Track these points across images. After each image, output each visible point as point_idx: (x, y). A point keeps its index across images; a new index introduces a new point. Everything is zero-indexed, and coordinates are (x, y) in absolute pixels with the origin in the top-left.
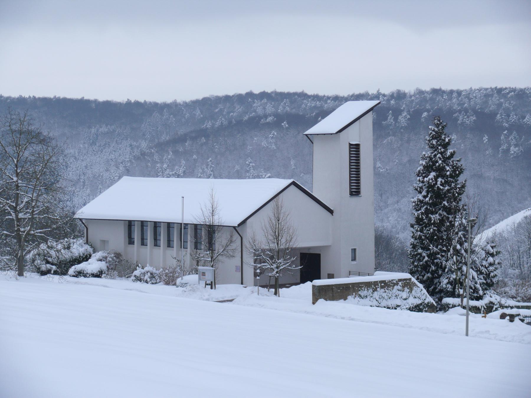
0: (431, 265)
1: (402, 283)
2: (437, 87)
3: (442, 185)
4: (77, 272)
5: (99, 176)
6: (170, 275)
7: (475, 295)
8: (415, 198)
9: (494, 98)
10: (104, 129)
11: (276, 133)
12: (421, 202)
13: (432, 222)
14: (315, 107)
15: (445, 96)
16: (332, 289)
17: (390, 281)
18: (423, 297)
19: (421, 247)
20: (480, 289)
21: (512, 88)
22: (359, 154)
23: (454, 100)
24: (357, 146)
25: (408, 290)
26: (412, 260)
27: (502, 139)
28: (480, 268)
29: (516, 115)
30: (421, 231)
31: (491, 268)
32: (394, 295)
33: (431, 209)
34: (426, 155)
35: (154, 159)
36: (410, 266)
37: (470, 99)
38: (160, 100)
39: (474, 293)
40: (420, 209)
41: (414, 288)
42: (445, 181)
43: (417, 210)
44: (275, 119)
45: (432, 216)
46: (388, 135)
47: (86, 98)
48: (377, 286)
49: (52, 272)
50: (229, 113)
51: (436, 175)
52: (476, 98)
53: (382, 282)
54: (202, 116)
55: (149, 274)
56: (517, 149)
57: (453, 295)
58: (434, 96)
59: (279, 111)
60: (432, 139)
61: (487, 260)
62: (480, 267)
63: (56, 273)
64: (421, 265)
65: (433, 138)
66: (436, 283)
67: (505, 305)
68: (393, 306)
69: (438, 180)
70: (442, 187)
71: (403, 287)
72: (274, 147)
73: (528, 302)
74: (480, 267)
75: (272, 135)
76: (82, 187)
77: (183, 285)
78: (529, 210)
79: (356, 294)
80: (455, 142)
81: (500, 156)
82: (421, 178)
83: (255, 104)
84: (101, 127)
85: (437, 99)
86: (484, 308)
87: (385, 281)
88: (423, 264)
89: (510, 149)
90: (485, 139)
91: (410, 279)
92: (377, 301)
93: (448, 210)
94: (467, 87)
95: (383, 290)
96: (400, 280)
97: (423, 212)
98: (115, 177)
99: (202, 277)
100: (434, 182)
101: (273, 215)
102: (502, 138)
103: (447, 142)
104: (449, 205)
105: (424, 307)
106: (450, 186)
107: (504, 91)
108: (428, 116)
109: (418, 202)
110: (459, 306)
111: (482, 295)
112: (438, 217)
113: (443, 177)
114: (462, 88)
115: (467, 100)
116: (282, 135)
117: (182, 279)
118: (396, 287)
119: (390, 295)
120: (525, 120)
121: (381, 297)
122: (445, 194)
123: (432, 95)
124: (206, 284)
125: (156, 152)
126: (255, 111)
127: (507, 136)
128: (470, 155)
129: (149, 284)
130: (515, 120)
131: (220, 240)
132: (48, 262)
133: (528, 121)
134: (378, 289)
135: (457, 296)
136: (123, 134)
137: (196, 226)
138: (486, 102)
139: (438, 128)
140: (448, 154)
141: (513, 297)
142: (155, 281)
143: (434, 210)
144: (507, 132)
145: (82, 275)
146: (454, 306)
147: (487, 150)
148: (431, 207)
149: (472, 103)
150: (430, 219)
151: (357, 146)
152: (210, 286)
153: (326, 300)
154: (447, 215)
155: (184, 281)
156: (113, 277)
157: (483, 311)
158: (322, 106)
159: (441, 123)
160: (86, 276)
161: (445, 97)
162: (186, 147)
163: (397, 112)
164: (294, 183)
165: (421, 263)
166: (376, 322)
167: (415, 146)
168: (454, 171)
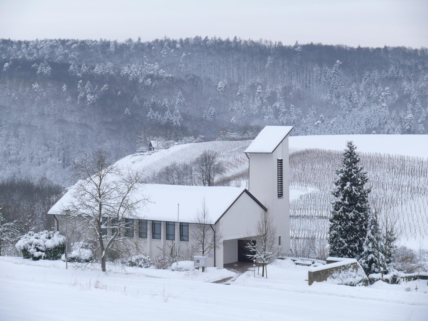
2: (7, 38)
4: (71, 258)
6: (162, 261)
15: (15, 46)
16: (320, 273)
21: (74, 40)
27: (78, 88)
29: (87, 66)
30: (340, 224)
32: (349, 275)
37: (38, 50)
40: (339, 209)
43: (337, 211)
45: (348, 214)
49: (43, 258)
53: (344, 266)
56: (93, 96)
58: (5, 47)
63: (44, 258)
64: (341, 250)
69: (352, 187)
71: (353, 269)
78: (134, 156)
80: (38, 90)
81: (78, 103)
85: (8, 49)
86: (391, 280)
87: (344, 265)
90: (64, 87)
91: (356, 263)
94: (34, 39)
96: (352, 264)
97: (342, 210)
99: (196, 263)
102: (79, 86)
109: (336, 203)
110: (380, 279)
114: (29, 39)
115: (35, 50)
117: (177, 265)
119: (347, 275)
120: (95, 70)
123: (3, 45)
127: (83, 85)
128: (52, 102)
129: (143, 268)
132: (38, 250)
134: (342, 271)
138: (52, 53)
144: (82, 82)
146: (377, 280)
147: (67, 97)
149: (40, 53)
150: (347, 216)
155: (179, 266)
157: (391, 282)
160: (80, 261)
161: (15, 47)
164: (246, 191)
165: (342, 248)
166: (374, 299)
167: (2, 93)
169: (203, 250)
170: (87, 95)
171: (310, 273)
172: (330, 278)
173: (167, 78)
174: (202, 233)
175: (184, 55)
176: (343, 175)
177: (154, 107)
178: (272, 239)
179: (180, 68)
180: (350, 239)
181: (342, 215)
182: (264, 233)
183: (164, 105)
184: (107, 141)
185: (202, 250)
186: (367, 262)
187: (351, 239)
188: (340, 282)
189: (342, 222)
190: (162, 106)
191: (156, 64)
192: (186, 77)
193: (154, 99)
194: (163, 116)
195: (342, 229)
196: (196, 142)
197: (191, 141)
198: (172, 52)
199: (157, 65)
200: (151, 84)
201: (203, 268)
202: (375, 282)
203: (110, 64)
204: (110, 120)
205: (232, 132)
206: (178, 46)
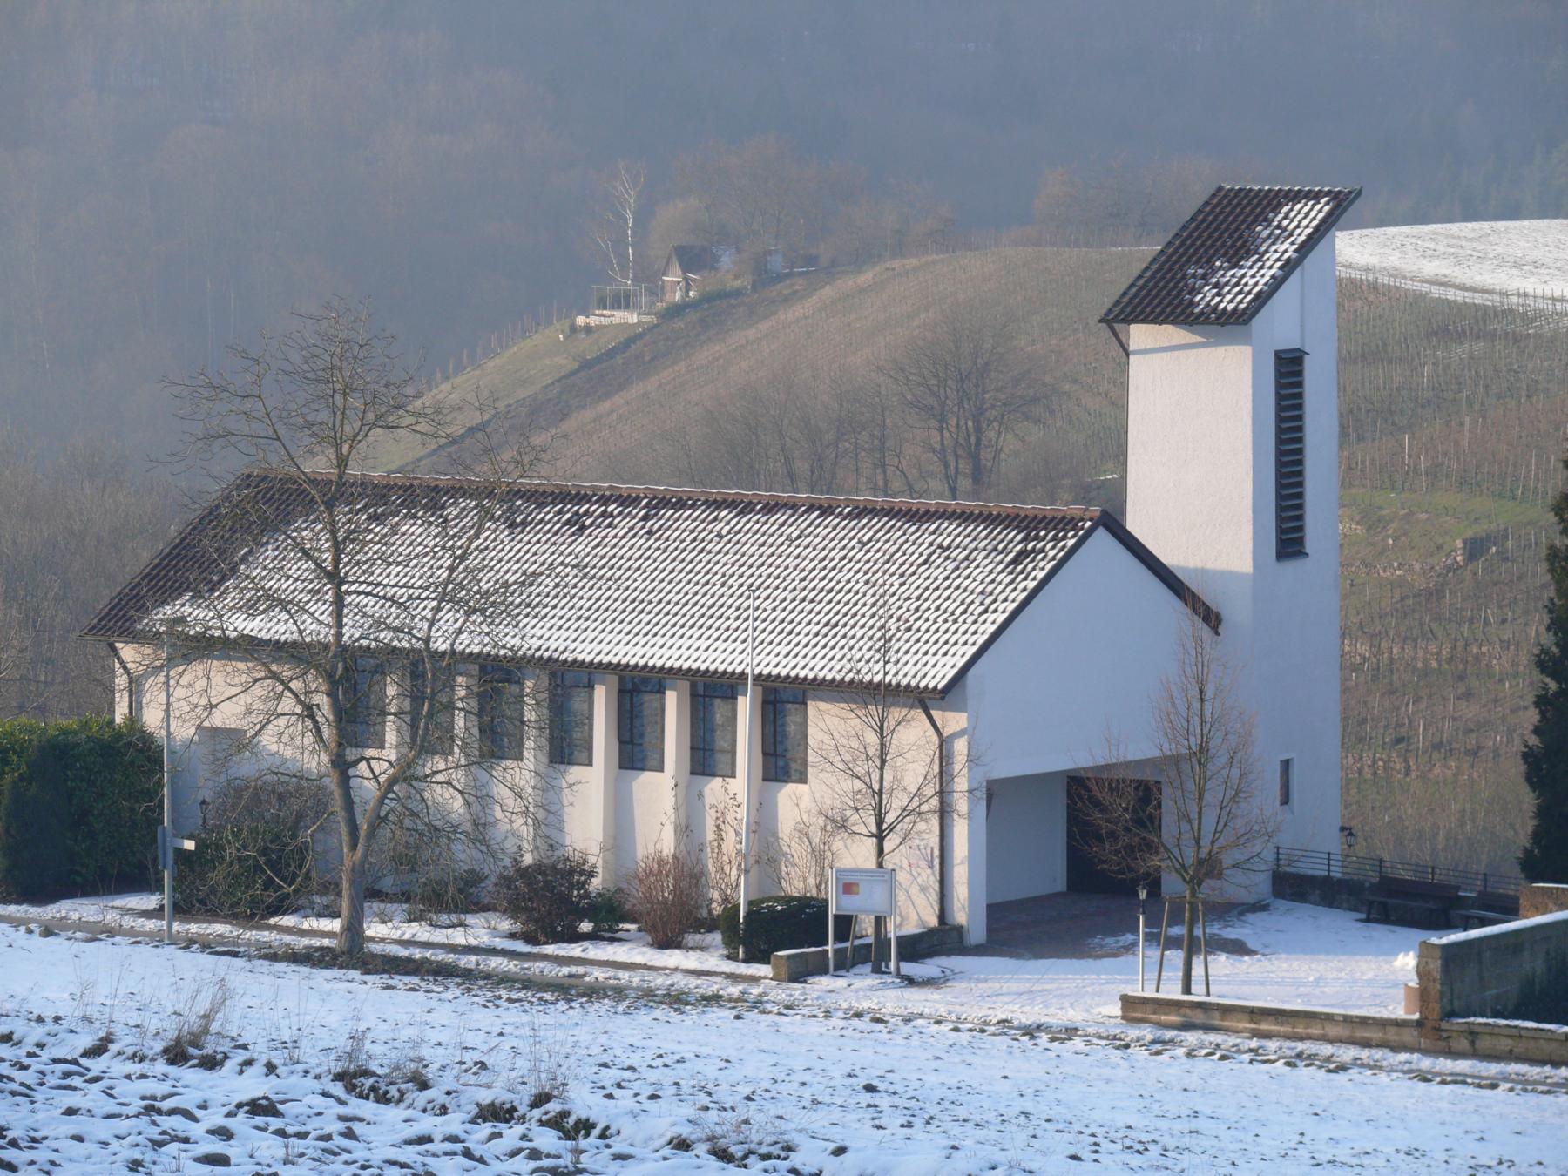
169: (880, 822)
174: (872, 738)
178: (1236, 772)
182: (1194, 742)
201: (1482, 1139)
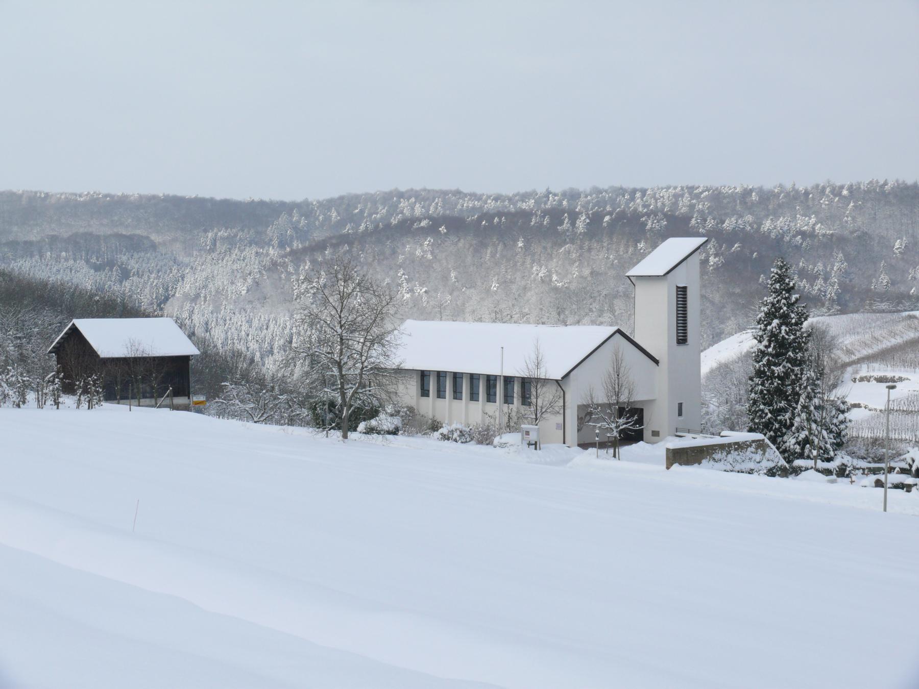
0: (774, 423)
1: (755, 445)
3: (787, 333)
5: (223, 290)
7: (826, 456)
8: (754, 348)
9: (685, 198)
10: (222, 233)
11: (432, 241)
12: (763, 352)
13: (776, 375)
14: (474, 208)
17: (743, 443)
18: (776, 460)
19: (762, 402)
20: (831, 449)
22: (686, 298)
23: (638, 201)
24: (684, 289)
25: (762, 452)
26: (751, 417)
28: (829, 427)
29: (714, 219)
30: (763, 384)
31: (842, 426)
33: (773, 360)
34: (768, 301)
35: (289, 270)
36: (749, 423)
37: (656, 200)
38: (287, 199)
39: (824, 454)
41: (767, 450)
42: (789, 329)
44: (431, 223)
46: (565, 243)
47: (201, 195)
48: (731, 449)
50: (370, 215)
51: (780, 322)
52: (664, 199)
54: (339, 218)
55: (458, 432)
56: (717, 259)
57: (801, 456)
59: (430, 212)
60: (774, 283)
61: (837, 418)
62: (830, 425)
64: (762, 423)
65: (776, 281)
66: (780, 442)
67: (857, 467)
68: (747, 470)
69: (782, 328)
70: (787, 337)
71: (757, 449)
72: (430, 257)
73: (878, 463)
74: (830, 425)
75: (428, 242)
76: (202, 303)
77: (503, 445)
78: (743, 333)
79: (710, 457)
80: (644, 250)
82: (762, 326)
83: (401, 204)
84: (220, 231)
86: (837, 471)
87: (739, 443)
88: (765, 421)
89: (709, 260)
91: (763, 440)
92: (731, 464)
93: (794, 362)
95: (736, 453)
96: (753, 441)
97: (765, 363)
98: (242, 291)
99: (525, 436)
100: (778, 331)
101: (612, 369)
103: (792, 287)
104: (794, 356)
105: (777, 470)
106: (795, 334)
107: (696, 189)
108: (610, 220)
109: (758, 353)
110: (812, 468)
111: (833, 456)
112: (782, 370)
113: (787, 325)
115: (653, 201)
116: (439, 242)
118: (749, 449)
119: (744, 458)
120: (724, 225)
121: (734, 460)
122: (790, 344)
124: (529, 444)
125: (291, 261)
126: (402, 212)
130: (713, 225)
131: (544, 396)
133: (728, 227)
134: (732, 452)
135: (806, 457)
136: (246, 239)
137: (523, 379)
139: (781, 270)
140: (793, 299)
141: (863, 458)
142: (465, 440)
143: (777, 361)
145: (375, 432)
146: (807, 469)
148: (773, 358)
150: (773, 372)
151: (684, 289)
152: (534, 446)
153: (681, 464)
154: (792, 368)
156: (411, 435)
158: (481, 207)
159: (785, 265)
162: (326, 256)
163: (574, 216)
164: (619, 331)
165: (764, 420)
167: (597, 255)
168: (799, 319)
170: (710, 257)
171: (668, 450)
172: (708, 460)
173: (824, 235)
175: (852, 204)
176: (768, 308)
177: (803, 274)
179: (847, 222)
180: (777, 408)
181: (764, 370)
183: (817, 272)
184: (732, 318)
185: (534, 417)
186: (798, 443)
187: (778, 407)
188: (729, 467)
189: (766, 381)
190: (814, 272)
191: (812, 217)
192: (852, 233)
193: (803, 263)
194: (812, 285)
195: (765, 392)
196: (830, 315)
197: (822, 313)
198: (836, 200)
199: (814, 218)
200: (802, 244)
202: (803, 472)
203: (749, 218)
204: (737, 290)
205: (882, 302)
206: (845, 192)
